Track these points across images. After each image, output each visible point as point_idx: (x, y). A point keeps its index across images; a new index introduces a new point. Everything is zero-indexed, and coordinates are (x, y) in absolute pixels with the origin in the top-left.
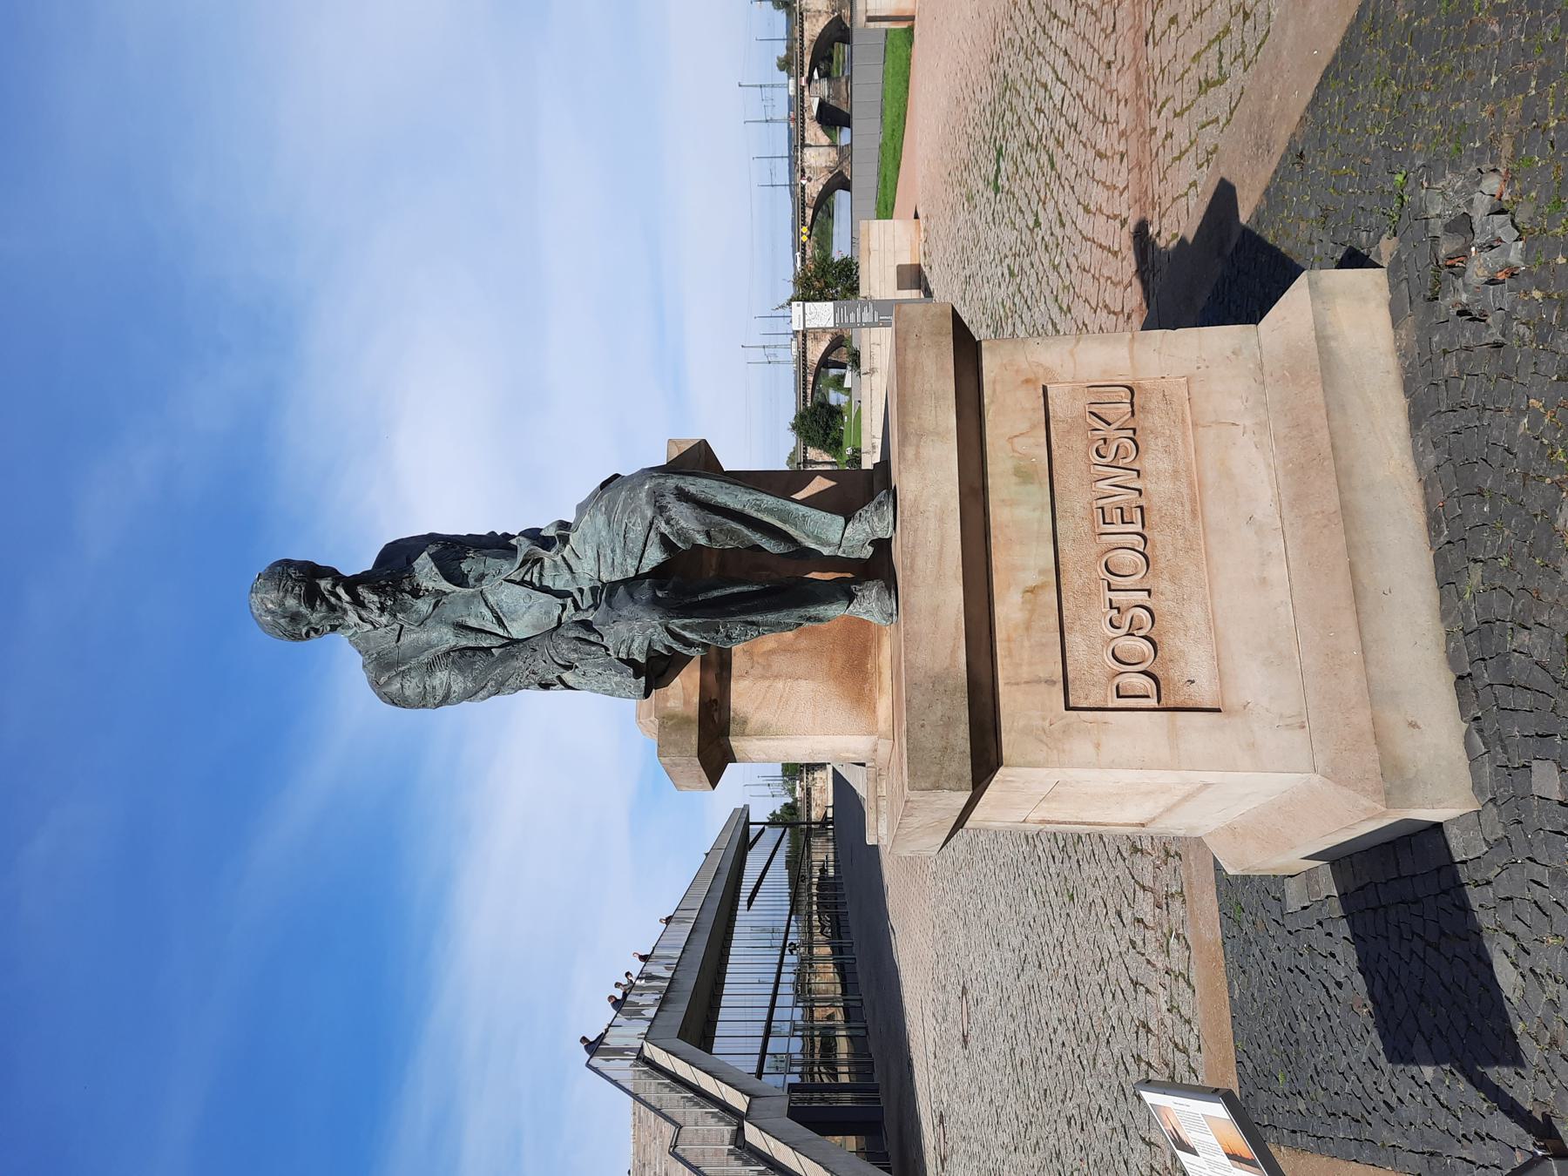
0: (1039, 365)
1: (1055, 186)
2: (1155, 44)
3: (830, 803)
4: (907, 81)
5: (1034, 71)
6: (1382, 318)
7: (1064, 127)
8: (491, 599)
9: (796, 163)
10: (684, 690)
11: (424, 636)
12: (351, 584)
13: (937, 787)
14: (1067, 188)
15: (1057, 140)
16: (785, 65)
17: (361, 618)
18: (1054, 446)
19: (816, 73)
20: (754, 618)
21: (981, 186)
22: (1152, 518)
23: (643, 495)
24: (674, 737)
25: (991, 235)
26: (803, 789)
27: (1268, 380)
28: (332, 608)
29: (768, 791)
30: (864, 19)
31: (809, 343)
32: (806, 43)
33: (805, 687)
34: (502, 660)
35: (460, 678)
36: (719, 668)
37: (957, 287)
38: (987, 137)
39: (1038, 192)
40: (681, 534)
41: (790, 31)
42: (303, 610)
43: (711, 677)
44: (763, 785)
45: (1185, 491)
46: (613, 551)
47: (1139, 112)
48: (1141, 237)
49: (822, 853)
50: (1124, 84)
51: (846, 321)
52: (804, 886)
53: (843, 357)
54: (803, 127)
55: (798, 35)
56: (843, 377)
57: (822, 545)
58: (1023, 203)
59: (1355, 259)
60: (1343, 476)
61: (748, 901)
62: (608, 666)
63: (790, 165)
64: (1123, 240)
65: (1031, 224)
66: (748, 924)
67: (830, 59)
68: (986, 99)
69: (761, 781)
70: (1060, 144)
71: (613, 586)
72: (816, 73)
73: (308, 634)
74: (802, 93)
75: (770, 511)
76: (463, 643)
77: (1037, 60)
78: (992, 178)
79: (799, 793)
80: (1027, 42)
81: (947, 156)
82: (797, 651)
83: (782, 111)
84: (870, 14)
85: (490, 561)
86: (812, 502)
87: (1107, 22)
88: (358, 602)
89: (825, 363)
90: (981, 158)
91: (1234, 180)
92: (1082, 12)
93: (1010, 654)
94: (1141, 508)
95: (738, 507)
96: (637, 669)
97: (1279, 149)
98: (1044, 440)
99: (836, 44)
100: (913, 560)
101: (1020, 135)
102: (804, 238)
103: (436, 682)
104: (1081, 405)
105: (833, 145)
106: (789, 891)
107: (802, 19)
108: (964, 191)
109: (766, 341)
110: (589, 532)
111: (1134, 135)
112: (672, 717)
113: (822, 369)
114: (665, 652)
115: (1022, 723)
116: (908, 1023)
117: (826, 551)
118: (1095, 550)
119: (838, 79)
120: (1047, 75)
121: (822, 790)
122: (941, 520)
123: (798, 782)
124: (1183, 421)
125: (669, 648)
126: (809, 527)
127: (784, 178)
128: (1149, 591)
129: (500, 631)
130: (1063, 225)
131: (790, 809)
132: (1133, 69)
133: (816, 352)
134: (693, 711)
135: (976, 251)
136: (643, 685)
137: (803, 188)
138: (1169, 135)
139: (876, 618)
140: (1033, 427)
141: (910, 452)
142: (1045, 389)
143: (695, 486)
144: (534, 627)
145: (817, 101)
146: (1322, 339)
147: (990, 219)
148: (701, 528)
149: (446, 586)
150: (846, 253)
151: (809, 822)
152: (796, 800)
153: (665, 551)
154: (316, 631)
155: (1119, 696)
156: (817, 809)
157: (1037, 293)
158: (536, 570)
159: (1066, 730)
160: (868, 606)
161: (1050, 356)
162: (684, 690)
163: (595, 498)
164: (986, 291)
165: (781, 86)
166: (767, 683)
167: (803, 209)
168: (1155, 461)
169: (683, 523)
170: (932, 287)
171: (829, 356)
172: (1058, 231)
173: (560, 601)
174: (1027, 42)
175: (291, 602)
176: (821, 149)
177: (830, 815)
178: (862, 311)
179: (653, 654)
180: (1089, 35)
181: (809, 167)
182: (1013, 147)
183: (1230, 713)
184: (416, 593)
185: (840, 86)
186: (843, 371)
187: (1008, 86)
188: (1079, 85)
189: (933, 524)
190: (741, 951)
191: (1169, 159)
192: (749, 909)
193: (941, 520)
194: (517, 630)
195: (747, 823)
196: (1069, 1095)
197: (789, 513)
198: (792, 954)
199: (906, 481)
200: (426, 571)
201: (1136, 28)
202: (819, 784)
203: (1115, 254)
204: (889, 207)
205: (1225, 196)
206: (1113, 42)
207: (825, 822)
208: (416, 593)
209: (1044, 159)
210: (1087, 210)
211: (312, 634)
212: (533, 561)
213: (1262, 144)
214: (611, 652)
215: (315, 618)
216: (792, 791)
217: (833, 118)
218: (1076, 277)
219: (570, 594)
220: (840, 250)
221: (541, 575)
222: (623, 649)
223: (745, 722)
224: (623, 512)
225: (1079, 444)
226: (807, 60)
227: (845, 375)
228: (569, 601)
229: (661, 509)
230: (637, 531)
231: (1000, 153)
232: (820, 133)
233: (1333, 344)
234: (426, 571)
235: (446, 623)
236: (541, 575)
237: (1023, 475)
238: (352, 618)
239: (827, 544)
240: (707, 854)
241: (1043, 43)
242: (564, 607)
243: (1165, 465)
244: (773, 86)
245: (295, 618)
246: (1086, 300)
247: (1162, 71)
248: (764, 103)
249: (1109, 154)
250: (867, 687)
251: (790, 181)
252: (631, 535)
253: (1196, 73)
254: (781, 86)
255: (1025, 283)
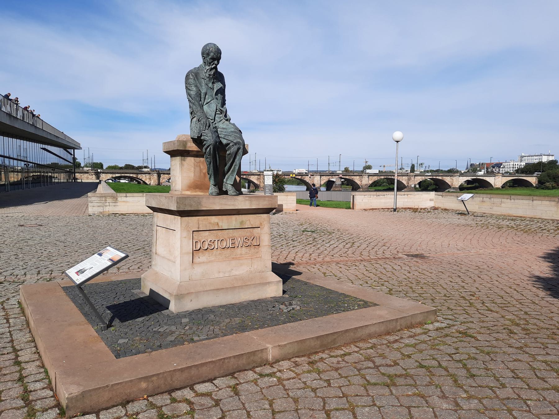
0: (264, 226)
1: (303, 245)
2: (336, 265)
3: (83, 181)
4: (336, 208)
5: (334, 239)
6: (273, 295)
7: (318, 247)
8: (212, 101)
9: (315, 173)
10: (192, 147)
11: (203, 85)
12: (216, 68)
13: (177, 203)
14: (302, 248)
15: (315, 245)
16: (346, 170)
17: (207, 70)
18: (248, 229)
19: (343, 180)
20: (212, 164)
21: (305, 227)
22: (232, 249)
23: (239, 140)
24: (182, 144)
25: (291, 230)
26: (87, 170)
27: (261, 273)
28: (210, 63)
29: (86, 157)
30: (354, 194)
31: (257, 176)
32: (352, 177)
33: (192, 175)
34: (199, 104)
35: (194, 94)
36: (196, 155)
37: (276, 221)
38: (318, 229)
39: (302, 241)
40: (230, 148)
41: (356, 172)
42: (210, 57)
43: (195, 153)
44: (89, 155)
45: (238, 256)
46: (225, 132)
47: (320, 262)
48: (291, 264)
49: (62, 178)
50: (327, 259)
51: (267, 188)
52: (50, 170)
53: (252, 188)
54: (327, 175)
55: (355, 174)
56: (245, 188)
57: (226, 179)
58: (299, 238)
59: (284, 292)
60: (241, 287)
61: (44, 148)
62: (200, 131)
63: (315, 171)
64: (289, 260)
65: (294, 240)
66: (28, 147)
67: (348, 185)
68: (328, 228)
69: (91, 154)
70: (314, 246)
71: (217, 132)
72: (343, 180)
73: (204, 56)
74: (337, 175)
75: (235, 168)
76: (202, 94)
77: (336, 240)
78: (307, 230)
79: (86, 169)
80: (341, 238)
81: (314, 218)
82: (201, 173)
83: (332, 169)
84: (355, 196)
85: (221, 101)
86: (235, 179)
87: (343, 255)
88: (211, 69)
89: (250, 182)
90: (312, 227)
91: (302, 275)
92: (347, 250)
93: (205, 219)
94: (234, 247)
95: (236, 161)
96: (199, 137)
97: (308, 281)
98: (249, 227)
99: (352, 187)
100: (225, 199)
101: (317, 237)
102: (291, 175)
103: (193, 87)
104: (256, 235)
105: (321, 186)
106: (46, 164)
107: (360, 176)
108: (303, 223)
109: (258, 162)
110: (229, 126)
111: (315, 262)
112: (186, 143)
113: (247, 181)
114: (204, 143)
115: (190, 221)
116: (13, 207)
117: (225, 180)
118: (226, 237)
119: (341, 187)
120: (332, 242)
121: (87, 178)
122: (233, 205)
123: (91, 169)
124: (252, 256)
125: (205, 145)
126: (230, 176)
127: (311, 169)
128: (217, 249)
129: (205, 103)
130: (293, 247)
131: (79, 165)
132: (331, 261)
133: (254, 179)
134: (187, 149)
135: (287, 226)
136: (195, 137)
137: (308, 175)
138: (314, 268)
139: (210, 191)
140: (252, 225)
141: (247, 198)
142: (259, 227)
143: (241, 151)
144: (206, 112)
145: (335, 180)
146: (269, 283)
147: (295, 230)
148: (231, 152)
149: (215, 90)
150: (286, 189)
151: (75, 173)
152: (83, 168)
153: (226, 144)
154: (204, 58)
155: (196, 242)
156: (80, 176)
157: (275, 241)
158: (219, 113)
159: (189, 231)
160: (213, 189)
161: (266, 229)
162: (192, 147)
163: (237, 128)
164: (276, 229)
165: (340, 169)
166: (193, 166)
167: (301, 175)
168: (244, 250)
169: (232, 149)
170: (276, 215)
171: (252, 184)
172: (292, 246)
173: (213, 119)
174: (341, 238)
175: (212, 54)
176: (320, 182)
177: (78, 181)
178: (269, 193)
179: (203, 141)
180: (340, 251)
181: (314, 178)
182: (315, 235)
183: (192, 265)
184: (213, 83)
185: (339, 188)
186: (247, 188)
187: (330, 233)
188: (329, 249)
189: (232, 203)
190: (15, 145)
191: (308, 268)
192: (41, 148)
193: (233, 205)
194: (205, 107)
195: (74, 149)
196: (25, 255)
197: (234, 172)
198: (25, 165)
199: (240, 198)
200: (218, 86)
201: (341, 261)
202: (90, 177)
203: (285, 259)
204: (300, 203)
205: (299, 273)
206: (338, 256)
207: (75, 179)
208: (213, 83)
209: (311, 242)
210: (297, 252)
211: (204, 57)
212: (221, 112)
213: (309, 279)
214: (204, 131)
215: (208, 59)
216: (86, 166)
217: (329, 185)
218: (280, 250)
219: (215, 121)
220: (287, 187)
221: (218, 114)
222: (205, 134)
223: (184, 160)
224: (235, 135)
225: (248, 234)
226: (347, 177)
227: (246, 189)
228: (213, 121)
229: (236, 144)
230: (231, 139)
231: (313, 232)
232: (325, 181)
233: (268, 285)
234: (218, 86)
235: (207, 90)
236: (218, 114)
237: (242, 223)
238: (208, 68)
239: (227, 180)
240: (63, 133)
241: (340, 241)
242: (212, 120)
243: (243, 252)
244: (340, 166)
245: (208, 54)
246: (273, 253)
247: (329, 266)
248: (334, 163)
249: (311, 257)
250: (192, 189)
251: (310, 171)
252: (229, 137)
253: (327, 272)
254: (340, 169)
255: (277, 238)
